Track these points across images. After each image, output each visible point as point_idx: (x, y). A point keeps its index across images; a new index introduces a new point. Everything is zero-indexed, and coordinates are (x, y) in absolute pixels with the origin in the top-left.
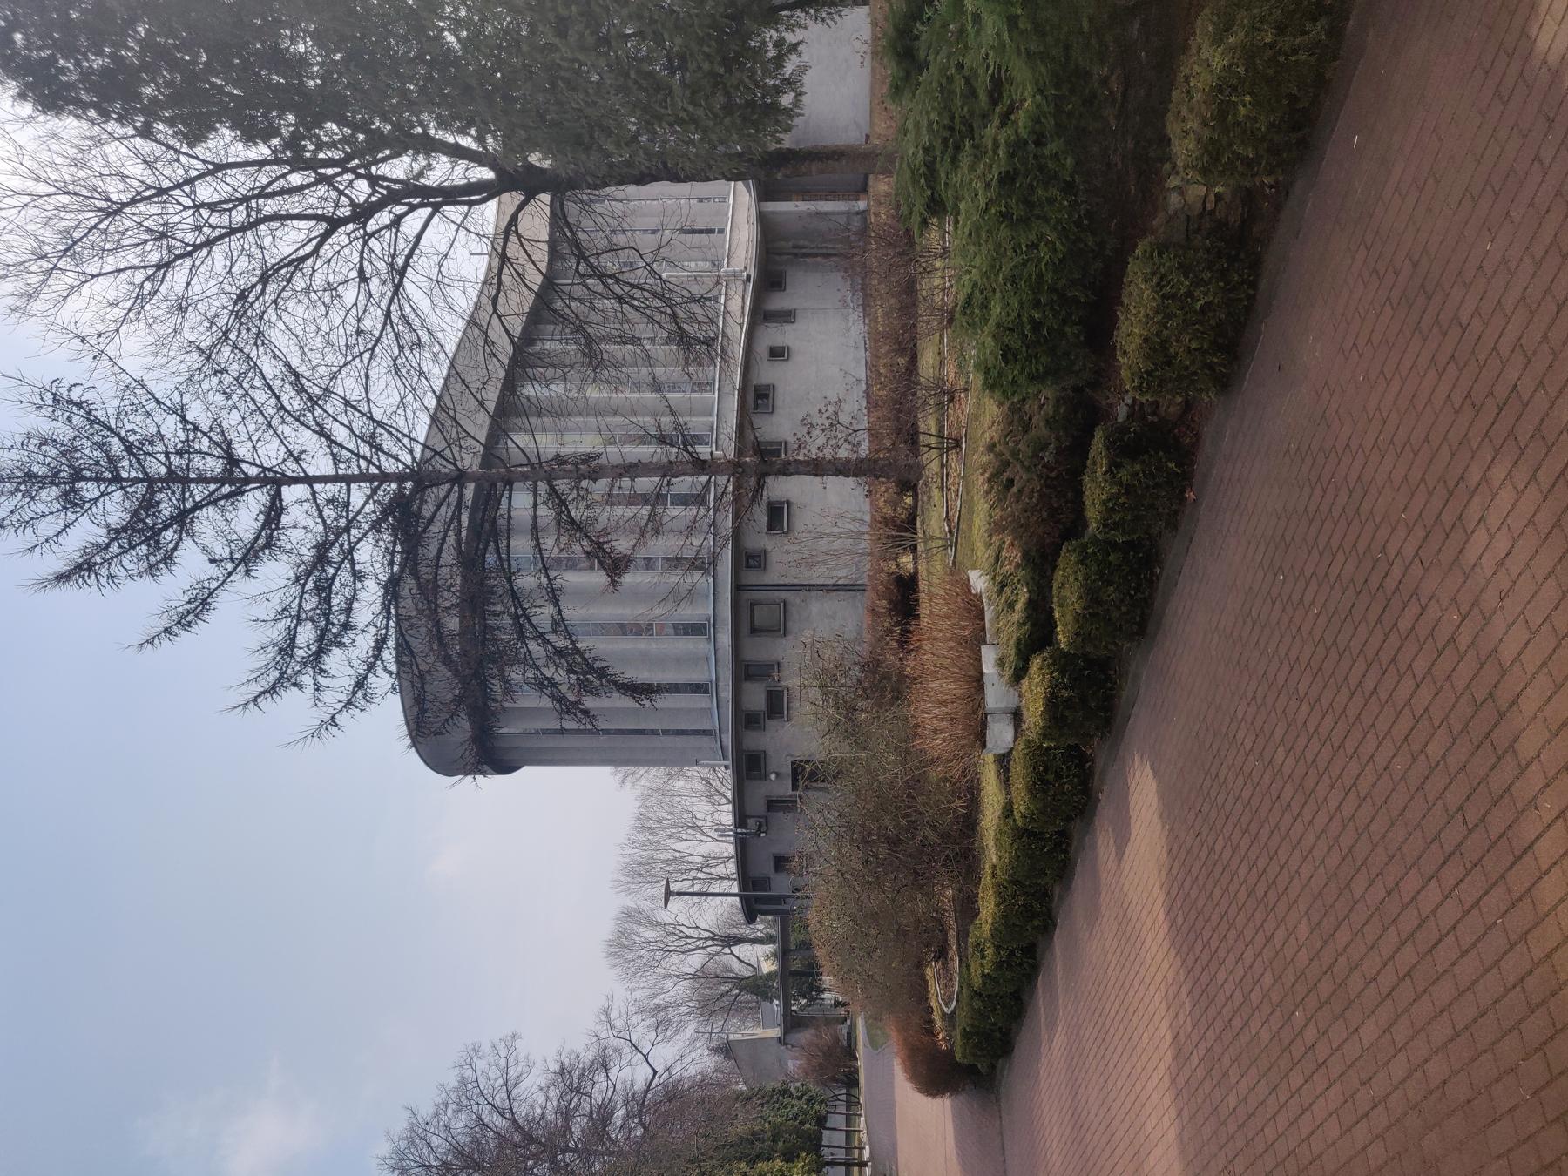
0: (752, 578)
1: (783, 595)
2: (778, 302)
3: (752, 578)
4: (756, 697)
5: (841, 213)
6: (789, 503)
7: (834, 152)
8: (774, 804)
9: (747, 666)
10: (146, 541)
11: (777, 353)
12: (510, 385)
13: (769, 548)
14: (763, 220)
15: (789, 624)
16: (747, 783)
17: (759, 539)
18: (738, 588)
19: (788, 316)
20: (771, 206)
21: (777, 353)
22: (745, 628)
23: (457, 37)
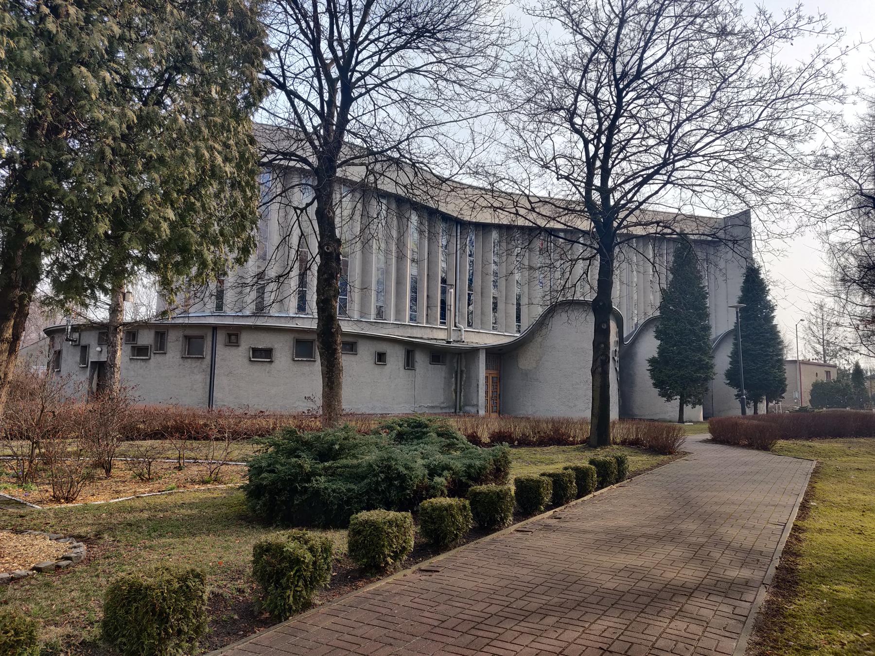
0: (221, 337)
1: (208, 358)
2: (421, 359)
3: (221, 337)
4: (146, 338)
5: (478, 401)
6: (271, 362)
7: (333, 383)
8: (85, 349)
9: (237, 335)
10: (208, 83)
11: (381, 358)
12: (418, 207)
13: (240, 348)
14: (475, 351)
15: (189, 360)
16: (98, 332)
17: (248, 341)
18: (215, 328)
19: (409, 364)
20: (482, 357)
21: (381, 358)
22: (189, 332)
23: (8, 225)
